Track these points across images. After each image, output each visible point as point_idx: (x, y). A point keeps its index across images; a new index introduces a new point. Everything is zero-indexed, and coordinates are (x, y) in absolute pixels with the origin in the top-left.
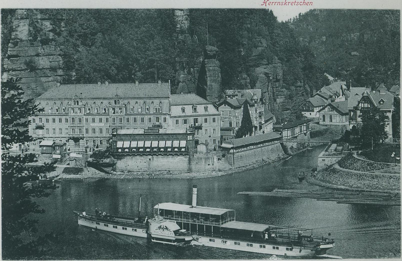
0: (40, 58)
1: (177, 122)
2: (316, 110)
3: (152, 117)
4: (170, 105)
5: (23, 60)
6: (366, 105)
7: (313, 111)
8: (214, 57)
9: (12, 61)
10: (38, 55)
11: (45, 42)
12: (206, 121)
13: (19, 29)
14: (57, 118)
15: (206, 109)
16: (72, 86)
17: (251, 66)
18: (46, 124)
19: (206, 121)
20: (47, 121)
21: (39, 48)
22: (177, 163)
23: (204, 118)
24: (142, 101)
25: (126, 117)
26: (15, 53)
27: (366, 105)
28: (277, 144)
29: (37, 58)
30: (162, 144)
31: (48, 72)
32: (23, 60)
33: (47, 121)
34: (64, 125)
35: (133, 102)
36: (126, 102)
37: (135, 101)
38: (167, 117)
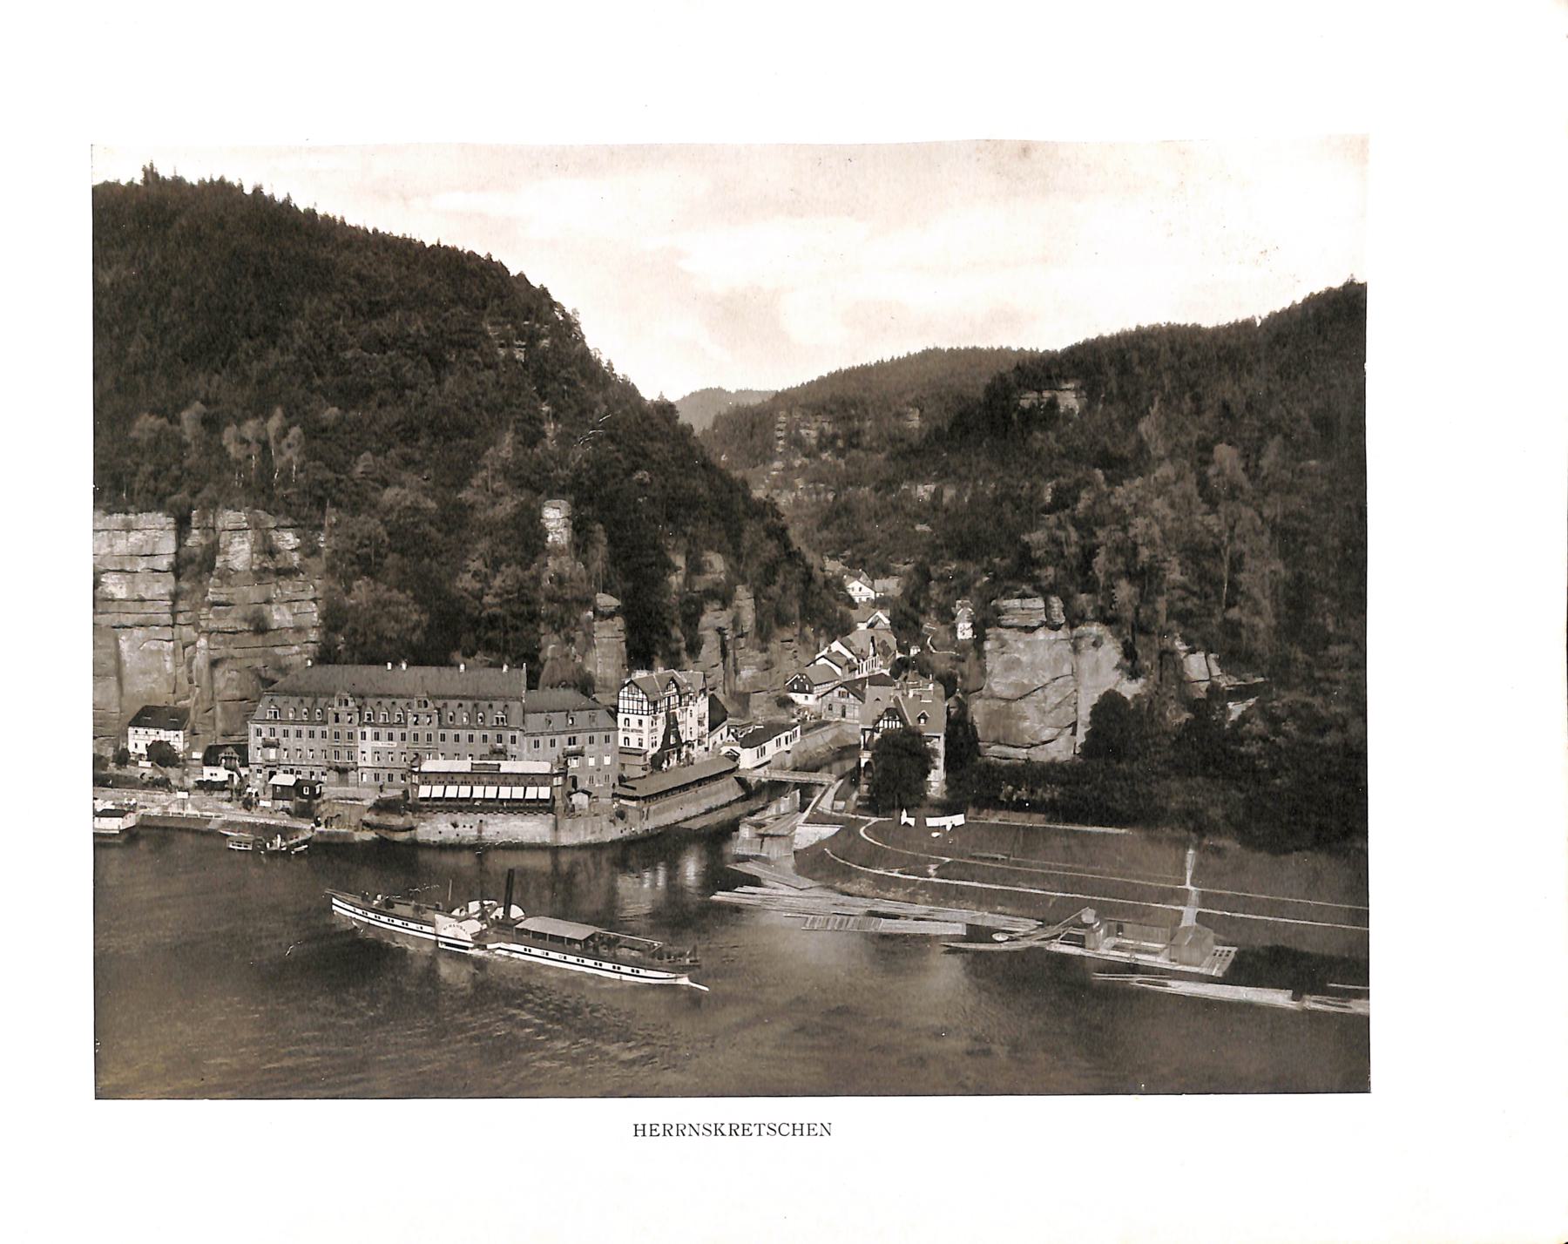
0: (274, 607)
1: (537, 744)
2: (819, 690)
3: (487, 733)
4: (525, 712)
5: (237, 612)
6: (892, 724)
7: (810, 692)
8: (611, 615)
9: (217, 614)
10: (268, 602)
11: (288, 573)
12: (591, 740)
13: (231, 549)
14: (305, 729)
15: (592, 719)
16: (336, 669)
17: (748, 507)
18: (283, 740)
19: (591, 740)
20: (286, 733)
21: (273, 587)
22: (531, 829)
23: (587, 735)
24: (470, 704)
25: (441, 731)
26: (223, 598)
27: (892, 724)
28: (731, 779)
29: (267, 608)
30: (505, 793)
31: (290, 637)
32: (237, 612)
33: (286, 733)
34: (318, 744)
35: (453, 703)
36: (440, 703)
37: (455, 703)
38: (518, 734)
